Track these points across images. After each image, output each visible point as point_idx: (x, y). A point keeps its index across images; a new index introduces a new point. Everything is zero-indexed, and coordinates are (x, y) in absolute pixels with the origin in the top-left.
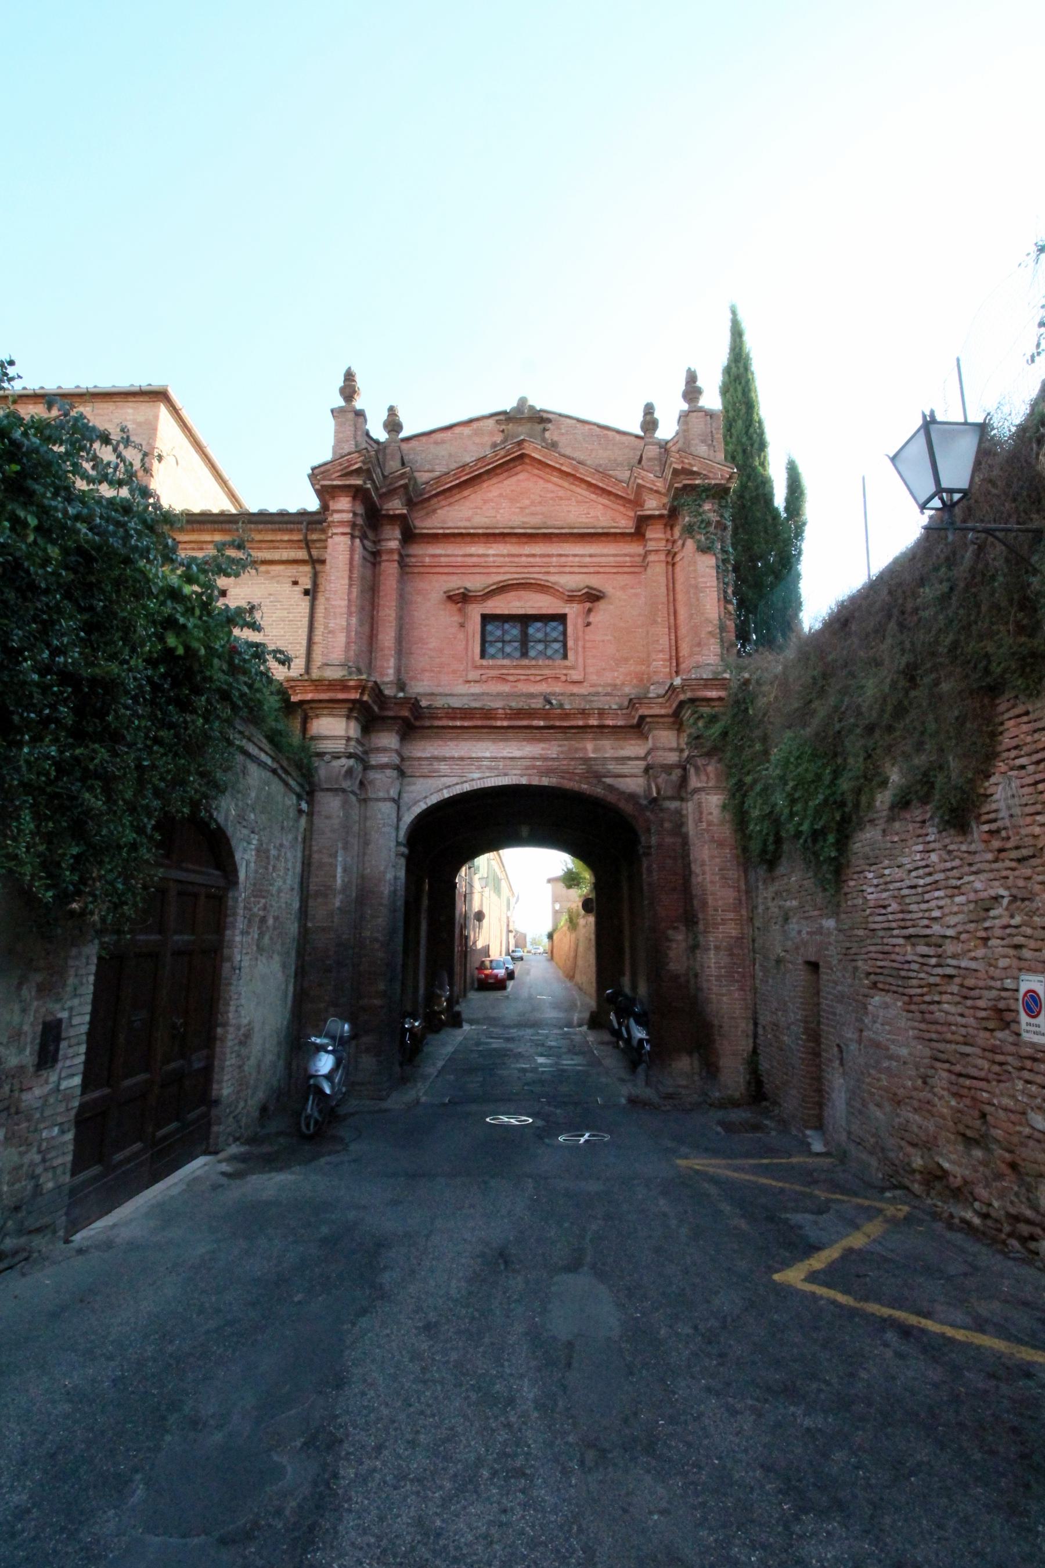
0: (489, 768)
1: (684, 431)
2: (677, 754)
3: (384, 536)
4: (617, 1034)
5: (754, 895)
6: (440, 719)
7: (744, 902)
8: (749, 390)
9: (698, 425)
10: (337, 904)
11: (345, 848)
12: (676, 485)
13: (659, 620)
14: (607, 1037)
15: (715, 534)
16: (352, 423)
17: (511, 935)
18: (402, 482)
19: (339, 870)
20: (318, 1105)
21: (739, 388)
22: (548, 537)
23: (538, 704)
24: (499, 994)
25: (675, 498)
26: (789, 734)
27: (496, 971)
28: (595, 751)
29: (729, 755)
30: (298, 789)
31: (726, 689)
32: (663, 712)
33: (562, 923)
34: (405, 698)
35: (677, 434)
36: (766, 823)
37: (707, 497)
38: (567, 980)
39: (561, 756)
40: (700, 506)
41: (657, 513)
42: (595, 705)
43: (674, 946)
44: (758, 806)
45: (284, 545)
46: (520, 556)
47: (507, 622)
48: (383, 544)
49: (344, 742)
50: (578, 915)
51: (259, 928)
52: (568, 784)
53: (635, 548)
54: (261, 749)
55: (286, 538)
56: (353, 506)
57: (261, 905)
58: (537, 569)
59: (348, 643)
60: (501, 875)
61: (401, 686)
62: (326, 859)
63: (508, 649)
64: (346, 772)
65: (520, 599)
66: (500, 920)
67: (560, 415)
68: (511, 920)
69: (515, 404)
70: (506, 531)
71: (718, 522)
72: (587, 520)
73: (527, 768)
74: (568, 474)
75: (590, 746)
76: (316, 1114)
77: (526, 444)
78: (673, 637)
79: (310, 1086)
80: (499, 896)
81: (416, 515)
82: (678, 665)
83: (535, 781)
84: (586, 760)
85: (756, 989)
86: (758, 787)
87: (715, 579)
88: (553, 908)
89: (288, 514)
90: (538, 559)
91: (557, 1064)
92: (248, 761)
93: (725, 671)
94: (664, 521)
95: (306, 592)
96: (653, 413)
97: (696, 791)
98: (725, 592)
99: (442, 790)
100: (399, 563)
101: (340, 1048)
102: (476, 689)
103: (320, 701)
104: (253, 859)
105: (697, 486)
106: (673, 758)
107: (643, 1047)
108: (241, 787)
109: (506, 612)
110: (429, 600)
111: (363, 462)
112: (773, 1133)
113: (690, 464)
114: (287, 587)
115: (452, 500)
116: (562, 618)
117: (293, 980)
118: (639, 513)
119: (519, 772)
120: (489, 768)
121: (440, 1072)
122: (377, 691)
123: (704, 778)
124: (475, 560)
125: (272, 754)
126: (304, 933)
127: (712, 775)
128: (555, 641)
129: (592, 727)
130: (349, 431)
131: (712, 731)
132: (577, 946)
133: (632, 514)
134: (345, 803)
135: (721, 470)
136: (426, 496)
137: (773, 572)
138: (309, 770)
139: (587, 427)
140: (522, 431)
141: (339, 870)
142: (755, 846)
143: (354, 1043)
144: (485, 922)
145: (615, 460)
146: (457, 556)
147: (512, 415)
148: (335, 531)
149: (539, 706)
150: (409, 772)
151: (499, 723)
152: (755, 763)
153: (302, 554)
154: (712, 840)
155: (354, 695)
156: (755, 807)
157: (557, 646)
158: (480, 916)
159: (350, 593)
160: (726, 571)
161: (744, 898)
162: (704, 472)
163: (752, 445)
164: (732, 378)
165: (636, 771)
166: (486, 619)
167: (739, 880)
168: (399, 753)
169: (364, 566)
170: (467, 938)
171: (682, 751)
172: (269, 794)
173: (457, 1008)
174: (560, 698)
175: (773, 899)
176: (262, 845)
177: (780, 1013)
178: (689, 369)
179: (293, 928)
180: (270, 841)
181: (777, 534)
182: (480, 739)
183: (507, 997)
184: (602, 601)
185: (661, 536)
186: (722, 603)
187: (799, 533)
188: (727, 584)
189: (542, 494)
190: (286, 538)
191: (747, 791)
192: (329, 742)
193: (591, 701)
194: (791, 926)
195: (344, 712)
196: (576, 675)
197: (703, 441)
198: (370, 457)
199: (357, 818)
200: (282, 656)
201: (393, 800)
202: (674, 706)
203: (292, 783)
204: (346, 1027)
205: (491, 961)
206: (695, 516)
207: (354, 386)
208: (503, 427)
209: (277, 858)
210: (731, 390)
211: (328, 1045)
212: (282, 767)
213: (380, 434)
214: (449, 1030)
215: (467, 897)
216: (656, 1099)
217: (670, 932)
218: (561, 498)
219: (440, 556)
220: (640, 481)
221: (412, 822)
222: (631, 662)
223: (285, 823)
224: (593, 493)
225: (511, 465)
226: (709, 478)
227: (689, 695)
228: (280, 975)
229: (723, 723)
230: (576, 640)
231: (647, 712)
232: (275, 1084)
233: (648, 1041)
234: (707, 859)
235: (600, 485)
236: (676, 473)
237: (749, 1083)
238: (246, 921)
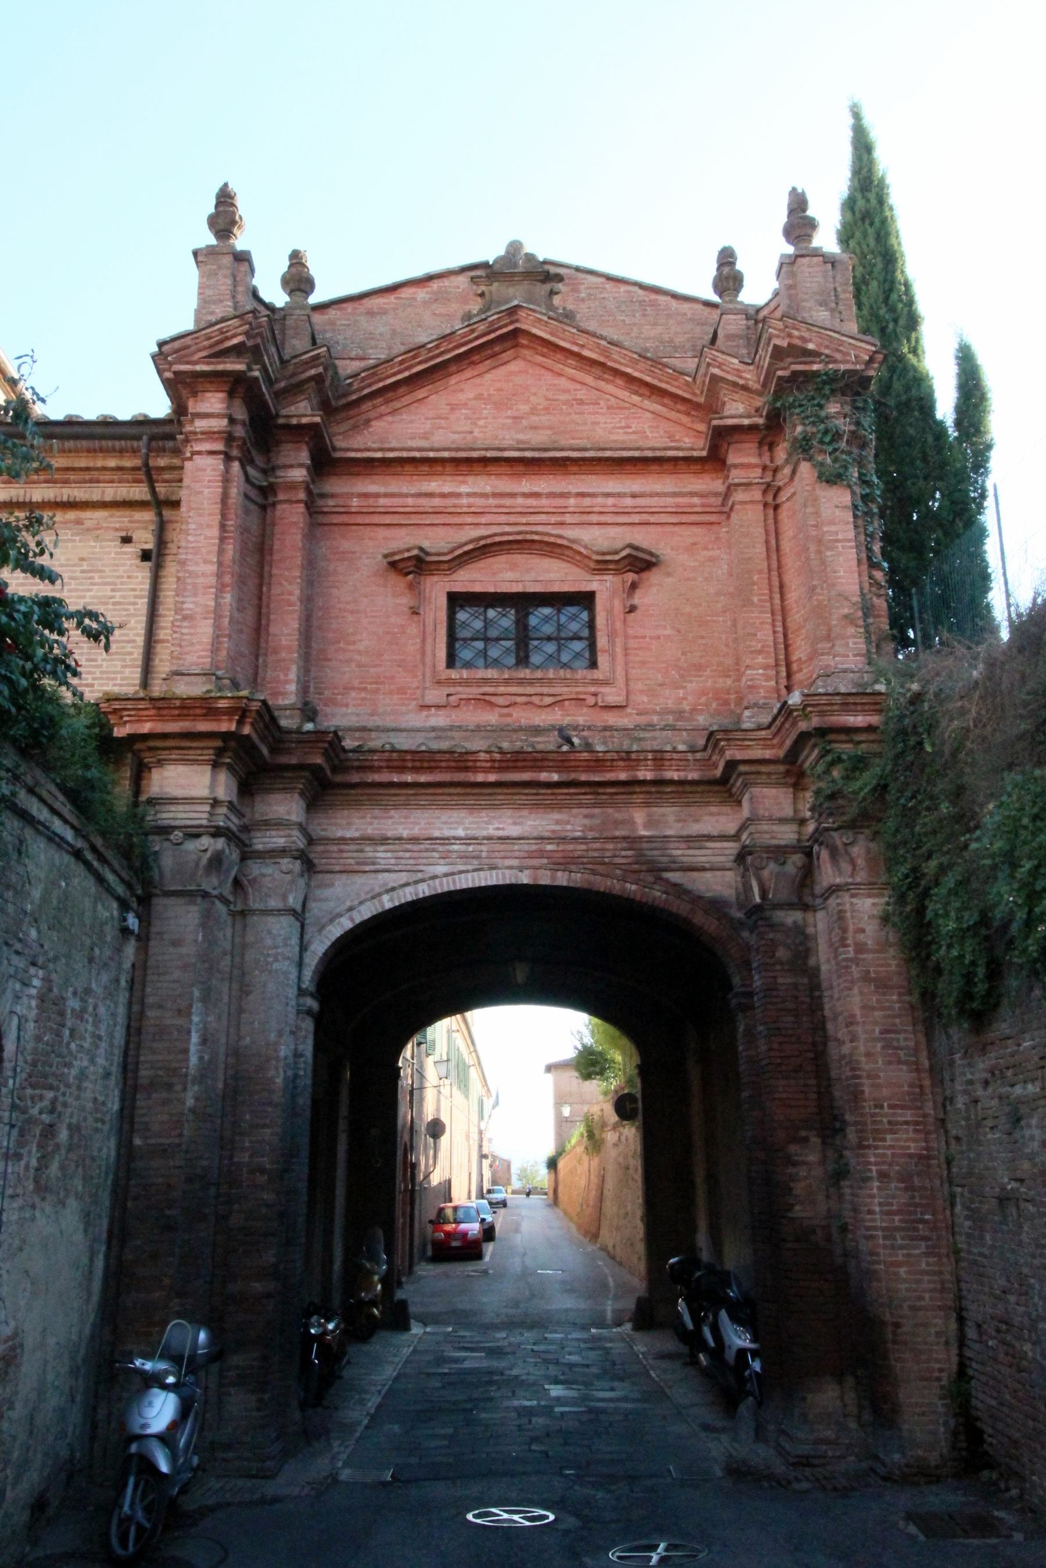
0: (464, 857)
1: (790, 287)
2: (794, 827)
3: (282, 460)
4: (692, 1340)
5: (947, 1076)
6: (379, 769)
7: (928, 1090)
8: (888, 234)
9: (811, 275)
10: (190, 1102)
11: (205, 999)
12: (780, 373)
13: (755, 599)
14: (669, 1343)
15: (849, 453)
16: (228, 272)
17: (486, 1163)
18: (313, 372)
19: (195, 1038)
20: (144, 1495)
21: (871, 231)
22: (561, 465)
23: (548, 743)
24: (470, 1268)
25: (778, 394)
26: (1010, 778)
27: (463, 1226)
28: (648, 825)
29: (891, 824)
30: (120, 890)
31: (880, 711)
32: (768, 754)
33: (574, 1141)
34: (316, 732)
35: (776, 294)
36: (970, 945)
37: (833, 391)
38: (586, 1241)
39: (590, 835)
40: (821, 407)
41: (746, 422)
42: (648, 745)
43: (803, 1172)
44: (953, 914)
45: (108, 476)
46: (512, 495)
47: (493, 606)
48: (280, 473)
49: (207, 808)
50: (604, 1125)
51: (40, 1146)
52: (603, 884)
53: (709, 483)
54: (54, 811)
55: (112, 463)
56: (228, 408)
57: (46, 1103)
58: (542, 518)
59: (217, 638)
60: (469, 1060)
61: (309, 712)
62: (171, 1020)
63: (494, 652)
64: (211, 861)
65: (513, 567)
66: (468, 1137)
67: (578, 269)
68: (486, 1136)
69: (502, 252)
70: (489, 454)
71: (853, 433)
72: (626, 437)
73: (531, 855)
74: (593, 362)
75: (639, 816)
76: (140, 1515)
77: (522, 314)
78: (780, 629)
79: (131, 1456)
80: (467, 1097)
81: (335, 429)
82: (789, 676)
83: (545, 879)
84: (633, 841)
85: (957, 1252)
86: (950, 881)
87: (852, 526)
88: (558, 1114)
89: (117, 423)
90: (544, 502)
91: (585, 1398)
92: (29, 833)
93: (876, 681)
94: (757, 437)
95: (146, 556)
96: (732, 264)
97: (834, 890)
98: (869, 550)
99: (380, 895)
100: (308, 507)
101: (190, 1379)
102: (439, 719)
103: (165, 736)
104: (33, 1014)
105: (816, 374)
106: (787, 835)
107: (747, 1366)
108: (14, 878)
109: (491, 589)
110: (358, 570)
111: (246, 333)
112: (1018, 1537)
113: (802, 338)
114: (113, 548)
115: (397, 404)
116: (586, 600)
117: (103, 1248)
118: (715, 422)
119: (515, 862)
120: (464, 857)
121: (373, 1418)
122: (267, 718)
123: (846, 867)
124: (437, 502)
125: (75, 822)
126: (127, 1154)
127: (861, 862)
128: (577, 638)
129: (643, 783)
130: (224, 284)
131: (859, 783)
132: (603, 1179)
133: (702, 427)
134: (207, 918)
135: (855, 347)
136: (354, 397)
137: (941, 525)
138: (144, 858)
139: (623, 288)
140: (515, 295)
141: (195, 1038)
142: (949, 989)
143: (215, 1367)
144: (444, 1140)
145: (671, 341)
146: (406, 496)
147: (497, 267)
148: (197, 447)
149: (551, 747)
150: (320, 862)
151: (480, 778)
152: (940, 837)
153: (139, 492)
154: (866, 978)
155: (227, 726)
156: (946, 915)
157: (578, 646)
158: (436, 1129)
159: (221, 552)
160: (868, 513)
161: (927, 1082)
162: (827, 351)
163: (896, 321)
164: (858, 215)
165: (722, 859)
166: (456, 600)
167: (916, 1049)
168: (303, 829)
169: (247, 512)
170: (414, 1166)
171: (802, 822)
172: (66, 896)
173: (400, 1295)
174: (585, 733)
175: (986, 1083)
176: (50, 990)
177: (1012, 1299)
178: (794, 189)
179: (106, 1148)
180: (67, 982)
181: (943, 464)
182: (445, 807)
183: (485, 1272)
184: (654, 570)
185: (754, 460)
186: (865, 567)
187: (980, 464)
188: (872, 536)
189: (550, 395)
190: (112, 463)
191: (928, 889)
192: (181, 808)
193: (640, 739)
194: (1027, 1133)
195: (209, 755)
196: (612, 695)
197: (823, 303)
198: (260, 326)
199: (227, 945)
200: (95, 625)
201: (293, 912)
202: (788, 743)
203: (110, 877)
204: (202, 1336)
205: (455, 1209)
206: (813, 423)
207: (234, 213)
208: (483, 288)
209: (80, 1015)
210: (858, 234)
211: (167, 1373)
212: (94, 849)
213: (276, 296)
214: (384, 1334)
215: (416, 1093)
216: (779, 1468)
217: (793, 1148)
218: (581, 402)
219: (377, 496)
220: (716, 371)
221: (325, 954)
222: (708, 672)
223: (97, 951)
224: (636, 393)
225: (497, 349)
226: (835, 361)
227: (816, 721)
228: (79, 1237)
229: (878, 770)
230: (612, 635)
231: (739, 755)
232: (64, 1453)
233: (755, 1353)
234: (858, 1012)
235: (648, 379)
236: (778, 353)
237: (955, 1434)
238: (15, 1132)
